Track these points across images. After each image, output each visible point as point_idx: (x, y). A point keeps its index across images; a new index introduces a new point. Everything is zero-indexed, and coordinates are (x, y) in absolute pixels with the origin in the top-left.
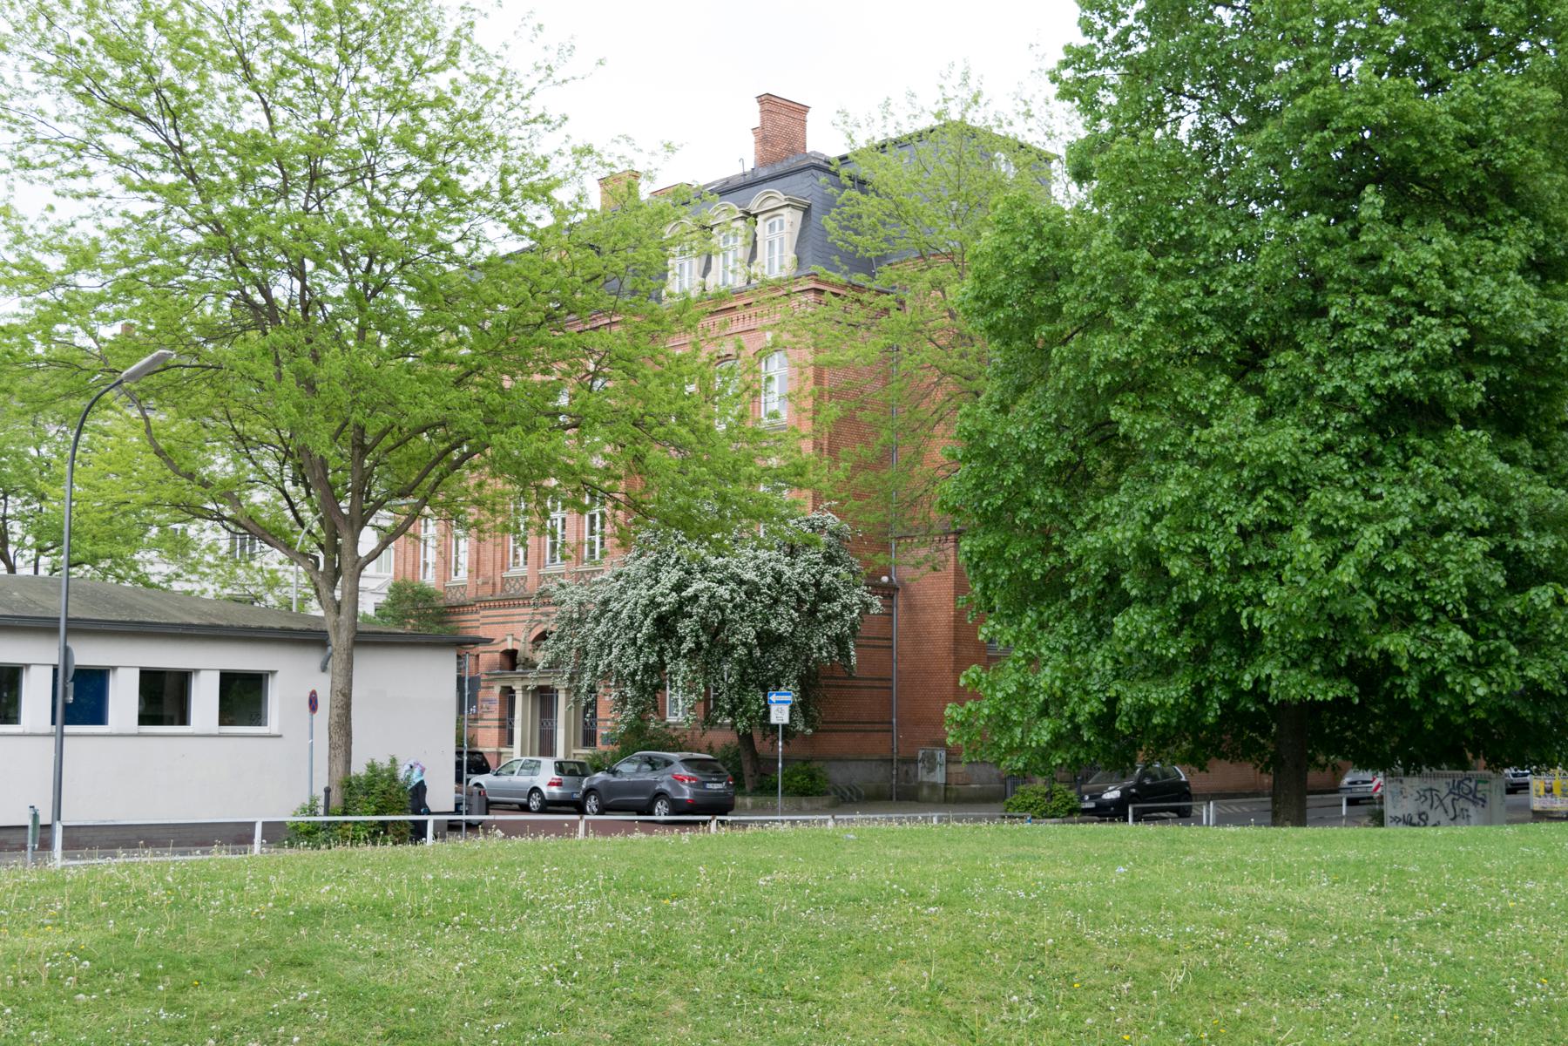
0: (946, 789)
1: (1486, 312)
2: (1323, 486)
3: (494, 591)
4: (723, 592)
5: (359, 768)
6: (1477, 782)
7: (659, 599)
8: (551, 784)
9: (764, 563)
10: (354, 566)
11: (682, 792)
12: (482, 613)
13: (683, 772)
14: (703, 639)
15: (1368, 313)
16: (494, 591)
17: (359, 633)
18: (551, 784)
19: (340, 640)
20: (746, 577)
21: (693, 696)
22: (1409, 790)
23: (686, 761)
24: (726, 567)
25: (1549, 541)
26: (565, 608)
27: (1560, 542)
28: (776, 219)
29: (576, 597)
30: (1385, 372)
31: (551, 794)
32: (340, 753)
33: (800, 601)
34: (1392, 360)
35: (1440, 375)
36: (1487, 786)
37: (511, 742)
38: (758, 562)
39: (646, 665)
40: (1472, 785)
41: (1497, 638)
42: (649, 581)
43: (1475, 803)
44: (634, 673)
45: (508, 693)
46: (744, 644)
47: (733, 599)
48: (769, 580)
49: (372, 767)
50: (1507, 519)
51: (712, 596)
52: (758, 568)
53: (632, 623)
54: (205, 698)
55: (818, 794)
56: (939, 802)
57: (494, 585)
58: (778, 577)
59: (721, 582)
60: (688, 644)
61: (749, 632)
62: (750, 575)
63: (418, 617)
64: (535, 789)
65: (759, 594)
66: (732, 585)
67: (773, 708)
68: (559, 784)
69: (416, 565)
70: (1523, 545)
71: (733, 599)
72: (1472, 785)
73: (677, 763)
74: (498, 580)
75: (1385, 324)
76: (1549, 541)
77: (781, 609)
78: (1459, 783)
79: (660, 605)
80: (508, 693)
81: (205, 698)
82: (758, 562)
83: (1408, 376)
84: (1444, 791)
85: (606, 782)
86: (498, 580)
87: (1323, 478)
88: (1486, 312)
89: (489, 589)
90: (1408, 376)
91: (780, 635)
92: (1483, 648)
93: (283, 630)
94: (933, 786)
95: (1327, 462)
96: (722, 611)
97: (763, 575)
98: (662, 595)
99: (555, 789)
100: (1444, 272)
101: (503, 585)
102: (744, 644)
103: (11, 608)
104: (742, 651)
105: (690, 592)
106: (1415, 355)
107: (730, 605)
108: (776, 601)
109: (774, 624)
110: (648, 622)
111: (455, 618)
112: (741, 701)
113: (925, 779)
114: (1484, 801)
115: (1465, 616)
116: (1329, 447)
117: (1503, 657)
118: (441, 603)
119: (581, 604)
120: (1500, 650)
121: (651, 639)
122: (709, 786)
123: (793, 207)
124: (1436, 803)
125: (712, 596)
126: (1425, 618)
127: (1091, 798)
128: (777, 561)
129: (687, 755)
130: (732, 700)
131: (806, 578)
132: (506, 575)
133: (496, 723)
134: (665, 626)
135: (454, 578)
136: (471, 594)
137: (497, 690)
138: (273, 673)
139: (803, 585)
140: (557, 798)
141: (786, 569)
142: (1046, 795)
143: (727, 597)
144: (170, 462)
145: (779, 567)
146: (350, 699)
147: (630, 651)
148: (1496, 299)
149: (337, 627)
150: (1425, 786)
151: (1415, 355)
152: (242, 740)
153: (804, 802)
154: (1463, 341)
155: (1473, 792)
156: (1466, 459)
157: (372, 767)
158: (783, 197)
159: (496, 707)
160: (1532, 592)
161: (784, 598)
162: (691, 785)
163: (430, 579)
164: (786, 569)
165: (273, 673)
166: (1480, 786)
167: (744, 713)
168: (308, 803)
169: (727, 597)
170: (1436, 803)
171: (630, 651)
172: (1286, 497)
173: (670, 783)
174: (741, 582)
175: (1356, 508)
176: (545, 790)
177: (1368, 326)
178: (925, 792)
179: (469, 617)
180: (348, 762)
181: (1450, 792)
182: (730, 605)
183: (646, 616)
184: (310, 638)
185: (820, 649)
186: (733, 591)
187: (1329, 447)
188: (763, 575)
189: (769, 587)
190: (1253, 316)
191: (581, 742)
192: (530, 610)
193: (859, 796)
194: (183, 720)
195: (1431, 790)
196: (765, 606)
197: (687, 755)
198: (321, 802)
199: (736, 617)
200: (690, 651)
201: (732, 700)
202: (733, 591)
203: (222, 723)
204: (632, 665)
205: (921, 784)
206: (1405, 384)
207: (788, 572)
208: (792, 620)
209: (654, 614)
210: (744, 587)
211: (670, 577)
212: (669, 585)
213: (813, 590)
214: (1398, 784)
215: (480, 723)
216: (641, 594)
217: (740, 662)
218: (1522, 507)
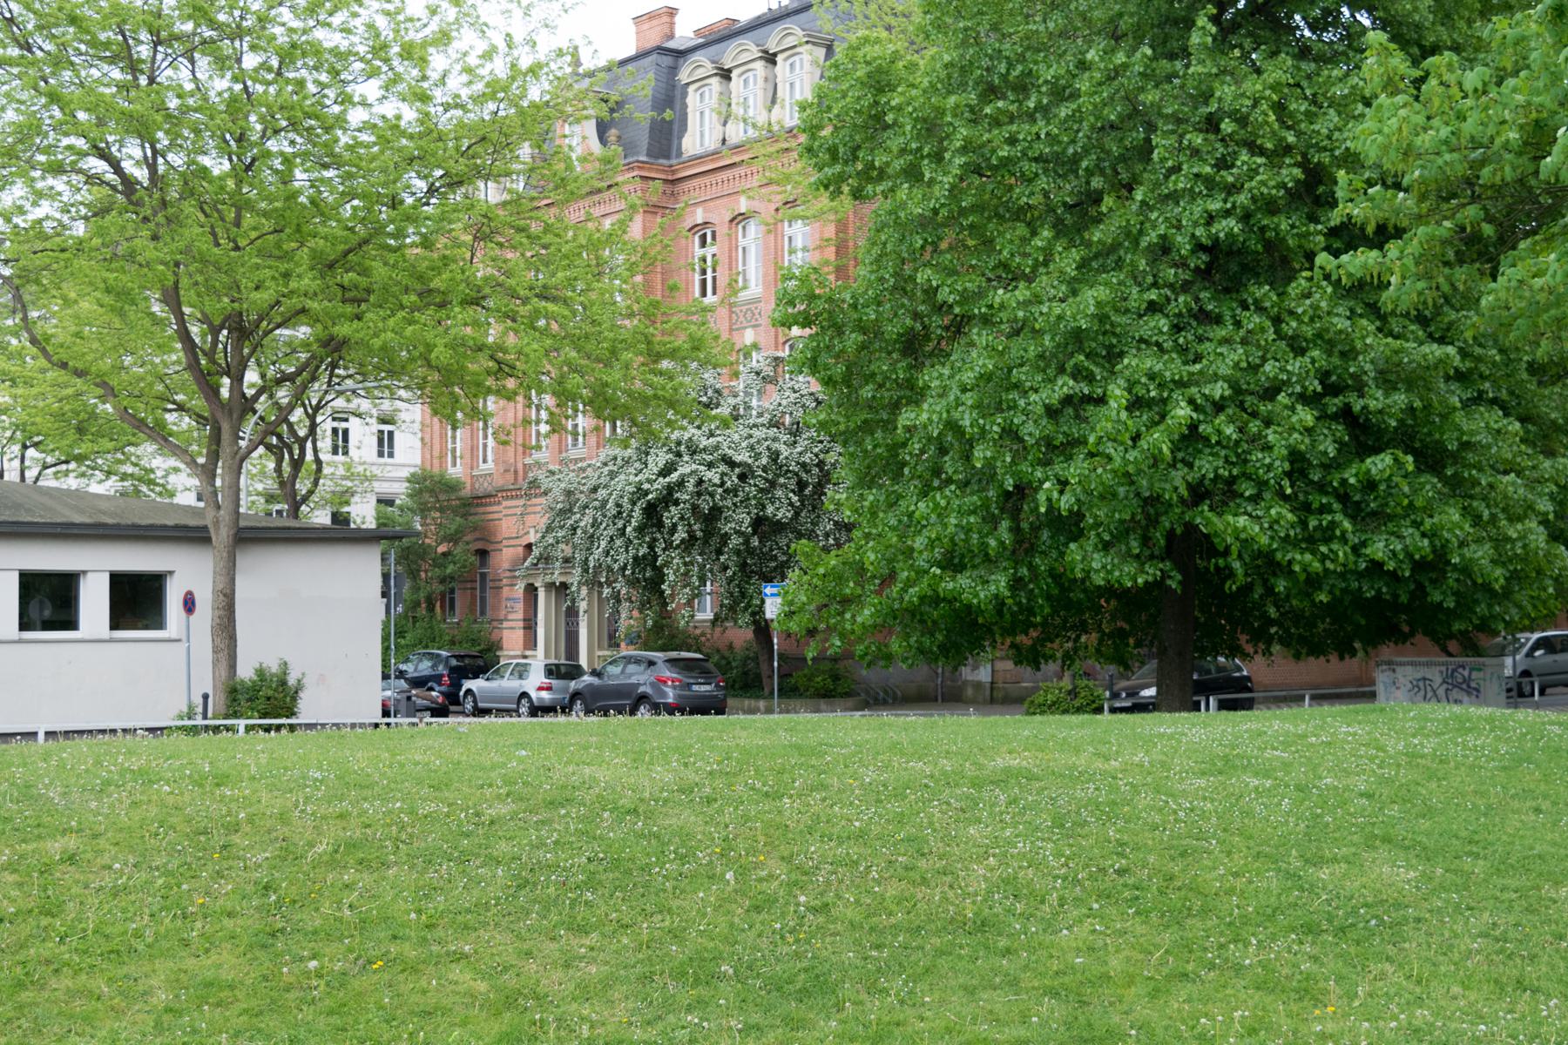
0: (992, 689)
1: (1325, 149)
2: (1139, 349)
3: (516, 479)
4: (713, 476)
5: (245, 672)
6: (1471, 670)
7: (646, 486)
8: (540, 689)
9: (758, 442)
10: (233, 458)
11: (664, 695)
12: (505, 503)
13: (667, 673)
14: (696, 527)
15: (1195, 152)
16: (516, 479)
17: (240, 530)
18: (540, 689)
19: (222, 536)
20: (738, 458)
21: (687, 590)
22: (1402, 680)
23: (672, 662)
24: (717, 447)
25: (1400, 399)
26: (550, 497)
27: (1411, 402)
28: (796, 58)
29: (563, 485)
30: (1210, 219)
31: (540, 699)
32: (223, 656)
33: (802, 485)
34: (1215, 205)
35: (1276, 220)
36: (1481, 675)
37: (534, 646)
38: (752, 441)
39: (636, 558)
40: (1466, 673)
41: (1331, 511)
42: (637, 465)
43: (1469, 694)
44: (624, 568)
45: (531, 590)
46: (738, 532)
47: (722, 484)
48: (764, 461)
49: (261, 672)
50: (1352, 376)
51: (700, 482)
52: (752, 448)
53: (620, 513)
54: (94, 601)
55: (847, 695)
56: (984, 703)
57: (516, 472)
58: (775, 456)
59: (710, 465)
60: (681, 534)
61: (744, 519)
62: (742, 457)
63: (441, 510)
64: (524, 695)
65: (754, 477)
66: (723, 468)
67: (768, 601)
68: (549, 689)
69: (442, 457)
70: (1373, 404)
71: (722, 484)
72: (1466, 673)
73: (660, 663)
74: (520, 466)
75: (1213, 166)
76: (1400, 399)
77: (779, 493)
78: (1454, 671)
79: (647, 493)
80: (531, 590)
81: (94, 601)
82: (752, 441)
83: (1232, 224)
84: (1438, 680)
85: (591, 685)
86: (520, 466)
87: (1141, 340)
88: (1325, 149)
89: (510, 477)
90: (1232, 224)
91: (779, 522)
92: (1313, 523)
93: (176, 527)
94: (978, 685)
95: (1146, 323)
96: (712, 495)
97: (757, 456)
98: (649, 481)
99: (545, 695)
100: (1279, 108)
101: (525, 473)
102: (738, 532)
103: (82, 512)
104: (735, 541)
105: (675, 476)
106: (1242, 199)
107: (720, 490)
108: (773, 484)
109: (770, 510)
110: (637, 513)
111: (481, 510)
112: (743, 594)
113: (970, 678)
114: (1478, 690)
115: (1289, 491)
116: (1153, 308)
117: (1338, 533)
118: (466, 492)
119: (569, 493)
120: (1333, 525)
121: (640, 530)
122: (695, 688)
123: (814, 44)
124: (1430, 694)
125: (700, 482)
126: (1247, 494)
127: (1129, 695)
128: (775, 440)
129: (674, 654)
130: (732, 594)
131: (807, 458)
132: (528, 461)
133: (521, 624)
134: (653, 513)
135: (482, 466)
136: (499, 482)
137: (520, 587)
138: (171, 573)
139: (804, 465)
140: (547, 703)
141: (783, 448)
142: (1069, 693)
143: (717, 481)
144: (44, 351)
145: (775, 446)
146: (233, 599)
147: (618, 542)
148: (1336, 135)
149: (217, 523)
150: (1419, 676)
151: (1242, 199)
152: (137, 640)
153: (822, 703)
154: (1298, 182)
155: (1467, 681)
156: (1304, 312)
157: (261, 672)
158: (800, 33)
159: (520, 607)
160: (1369, 461)
161: (782, 480)
162: (674, 687)
163: (456, 471)
164: (783, 448)
165: (171, 573)
166: (1475, 675)
167: (746, 609)
168: (185, 710)
169: (717, 481)
170: (1430, 694)
171: (618, 542)
172: (1097, 364)
173: (652, 684)
174: (731, 464)
175: (1168, 374)
176: (534, 695)
177: (1195, 170)
178: (970, 692)
179: (495, 508)
180: (232, 666)
181: (1444, 682)
182: (720, 490)
183: (634, 503)
184: (191, 535)
185: (827, 535)
186: (723, 474)
187: (1153, 308)
188: (757, 456)
189: (765, 469)
190: (1084, 164)
191: (606, 643)
192: (521, 502)
193: (895, 699)
194: (70, 623)
195: (1424, 679)
196: (761, 490)
197: (674, 654)
198: (200, 709)
199: (729, 503)
200: (683, 541)
201: (732, 594)
202: (723, 474)
203: (114, 625)
204: (622, 558)
205: (966, 682)
206: (1230, 234)
207: (785, 452)
208: (791, 504)
209: (641, 504)
210: (737, 470)
211: (659, 458)
212: (655, 470)
213: (816, 470)
214: (1389, 673)
215: (505, 624)
216: (625, 482)
217: (738, 553)
218: (1365, 364)
